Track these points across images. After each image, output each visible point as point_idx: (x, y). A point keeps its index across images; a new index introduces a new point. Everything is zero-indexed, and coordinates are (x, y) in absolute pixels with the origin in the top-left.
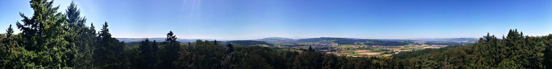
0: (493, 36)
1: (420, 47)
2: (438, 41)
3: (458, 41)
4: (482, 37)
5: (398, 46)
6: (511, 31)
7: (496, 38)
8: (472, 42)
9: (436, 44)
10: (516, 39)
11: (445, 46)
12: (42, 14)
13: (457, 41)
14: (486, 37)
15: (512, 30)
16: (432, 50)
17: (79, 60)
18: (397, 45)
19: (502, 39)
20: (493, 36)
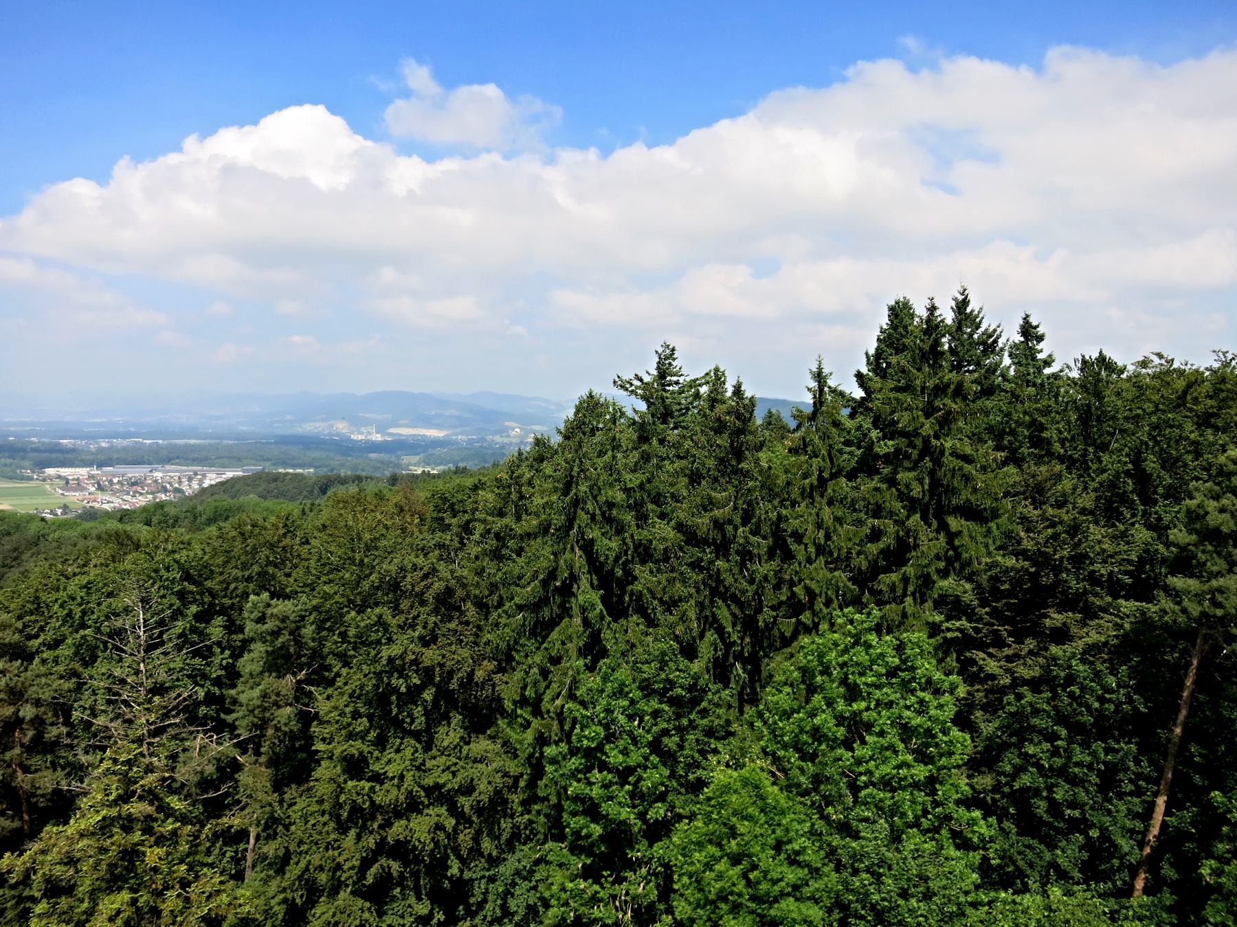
0: (717, 378)
1: (186, 471)
2: (120, 420)
3: (357, 423)
4: (608, 392)
5: (77, 466)
6: (899, 312)
7: (738, 391)
8: (503, 431)
9: (102, 460)
10: (959, 392)
11: (211, 479)
12: (886, 455)
13: (342, 427)
14: (646, 386)
15: (921, 311)
16: (36, 541)
17: (645, 443)
18: (101, 457)
19: (809, 399)
20: (717, 378)
